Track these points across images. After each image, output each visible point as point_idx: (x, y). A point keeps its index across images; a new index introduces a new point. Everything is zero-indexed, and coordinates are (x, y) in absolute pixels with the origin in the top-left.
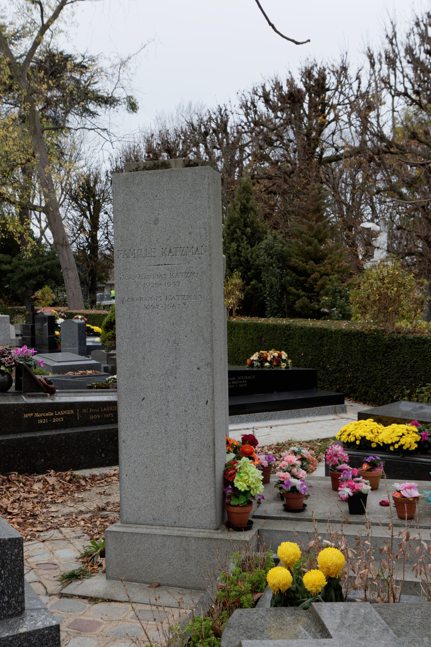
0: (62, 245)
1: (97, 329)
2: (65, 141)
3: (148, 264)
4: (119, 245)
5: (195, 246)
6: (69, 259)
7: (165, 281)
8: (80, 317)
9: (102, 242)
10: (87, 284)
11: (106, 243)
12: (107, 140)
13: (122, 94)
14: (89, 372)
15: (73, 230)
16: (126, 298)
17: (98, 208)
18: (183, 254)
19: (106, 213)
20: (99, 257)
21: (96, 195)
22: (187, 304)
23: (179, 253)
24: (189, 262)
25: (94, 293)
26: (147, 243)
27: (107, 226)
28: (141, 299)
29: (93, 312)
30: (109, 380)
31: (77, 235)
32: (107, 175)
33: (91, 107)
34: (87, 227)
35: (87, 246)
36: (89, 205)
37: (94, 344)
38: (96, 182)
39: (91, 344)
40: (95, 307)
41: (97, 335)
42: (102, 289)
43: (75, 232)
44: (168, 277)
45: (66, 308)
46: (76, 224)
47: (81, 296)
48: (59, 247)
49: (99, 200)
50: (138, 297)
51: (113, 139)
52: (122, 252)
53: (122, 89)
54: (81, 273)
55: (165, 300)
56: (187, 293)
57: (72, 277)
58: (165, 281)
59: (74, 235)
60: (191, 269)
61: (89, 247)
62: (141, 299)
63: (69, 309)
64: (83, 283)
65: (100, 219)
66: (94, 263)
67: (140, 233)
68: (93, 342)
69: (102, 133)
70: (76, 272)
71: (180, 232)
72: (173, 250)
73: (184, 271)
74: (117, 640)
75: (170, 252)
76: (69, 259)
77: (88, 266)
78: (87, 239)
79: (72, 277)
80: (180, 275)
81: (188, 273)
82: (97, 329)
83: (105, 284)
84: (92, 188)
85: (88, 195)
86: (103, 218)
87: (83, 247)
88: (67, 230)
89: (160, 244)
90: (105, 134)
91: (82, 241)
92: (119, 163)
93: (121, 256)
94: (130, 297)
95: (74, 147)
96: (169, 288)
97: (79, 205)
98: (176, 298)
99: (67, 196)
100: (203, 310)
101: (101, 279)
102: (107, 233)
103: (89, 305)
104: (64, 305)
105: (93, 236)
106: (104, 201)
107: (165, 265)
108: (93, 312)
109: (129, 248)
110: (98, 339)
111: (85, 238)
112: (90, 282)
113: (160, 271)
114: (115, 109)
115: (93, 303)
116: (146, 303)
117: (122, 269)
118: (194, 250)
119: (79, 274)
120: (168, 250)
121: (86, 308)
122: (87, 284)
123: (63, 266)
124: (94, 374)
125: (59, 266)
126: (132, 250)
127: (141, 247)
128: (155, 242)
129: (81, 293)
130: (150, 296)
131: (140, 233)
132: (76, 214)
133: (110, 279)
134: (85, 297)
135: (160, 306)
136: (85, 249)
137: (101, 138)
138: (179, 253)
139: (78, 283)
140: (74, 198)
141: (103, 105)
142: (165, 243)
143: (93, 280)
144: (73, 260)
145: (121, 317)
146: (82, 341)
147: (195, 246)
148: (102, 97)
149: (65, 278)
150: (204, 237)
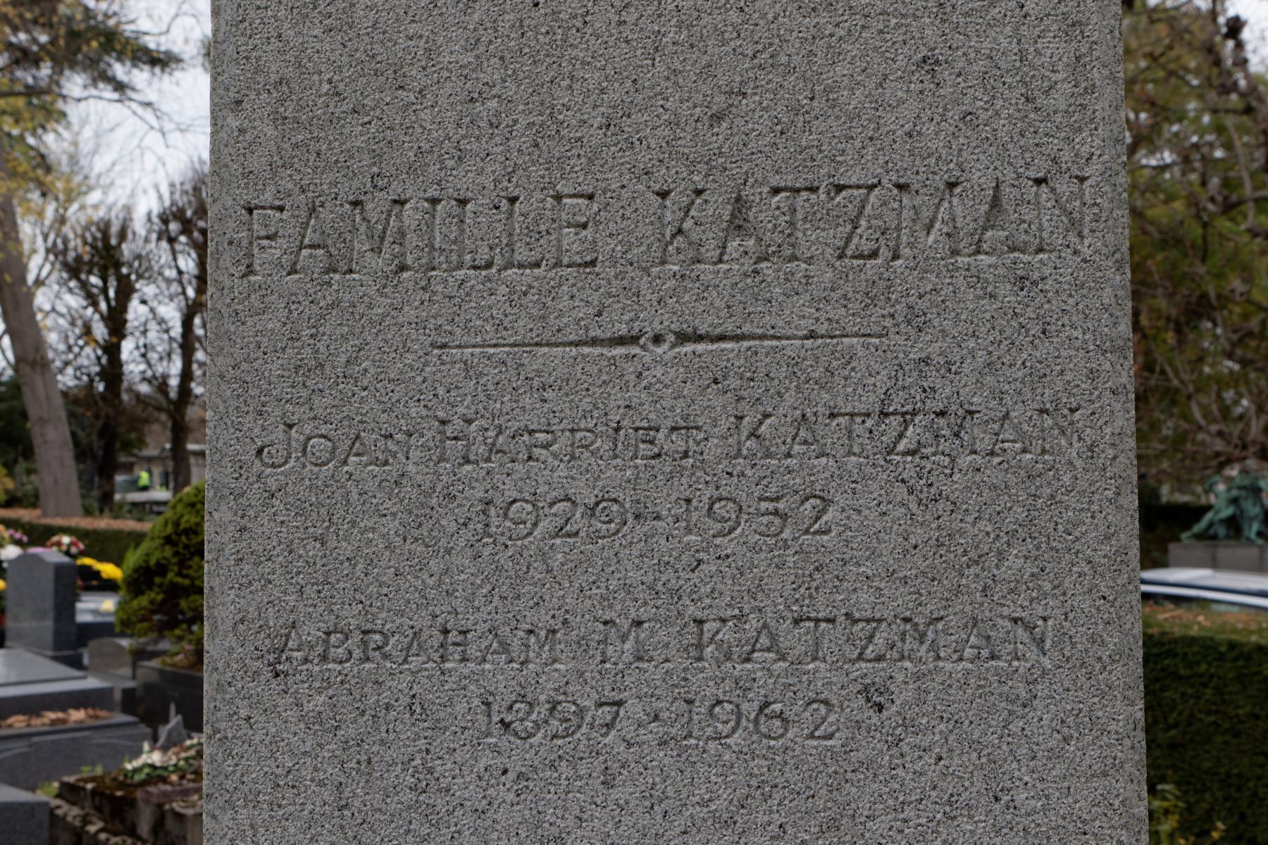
0: (33, 364)
1: (109, 570)
2: (53, 142)
3: (523, 327)
4: (257, 163)
5: (980, 177)
6: (48, 398)
7: (681, 488)
8: (66, 540)
9: (133, 365)
10: (94, 457)
11: (143, 367)
12: (152, 128)
13: (192, 29)
14: (77, 715)
15: (67, 337)
16: (311, 631)
17: (125, 291)
18: (861, 242)
19: (144, 302)
20: (125, 397)
21: (123, 264)
22: (905, 695)
23: (818, 240)
24: (917, 321)
25: (110, 478)
26: (521, 141)
27: (144, 332)
28: (451, 638)
29: (103, 523)
30: (136, 771)
31: (76, 349)
32: (149, 220)
33: (120, 70)
34: (100, 331)
35: (98, 374)
36: (105, 281)
37: (99, 619)
38: (122, 235)
39: (88, 618)
40: (111, 510)
41: (108, 586)
42: (129, 468)
43: (72, 341)
44: (713, 449)
45: (38, 512)
46: (73, 324)
47: (75, 486)
48: (26, 369)
49: (128, 276)
50: (422, 621)
51: (168, 126)
52: (287, 223)
53: (193, 21)
54: (81, 434)
55: (680, 662)
56: (899, 600)
57: (54, 441)
58: (681, 488)
59: (70, 348)
60: (934, 379)
61: (103, 374)
62: (451, 638)
63: (45, 515)
64: (82, 453)
65: (130, 316)
66: (111, 411)
67: (453, 53)
68: (96, 612)
69: (140, 110)
70: (65, 430)
71: (835, 57)
72: (767, 213)
73: (870, 402)
74: (148, 225)
75: (738, 225)
76: (48, 398)
77: (97, 417)
78: (99, 358)
79: (54, 441)
80: (832, 433)
81: (907, 418)
82: (109, 570)
83: (135, 456)
84: (114, 248)
85: (102, 262)
86: (136, 312)
87: (89, 375)
88: (52, 338)
89: (644, 158)
90: (148, 115)
91: (86, 362)
92: (177, 196)
93: (275, 251)
94: (351, 617)
95: (73, 159)
96: (727, 545)
97: (84, 285)
98: (795, 640)
99: (58, 266)
100: (1054, 755)
101: (127, 446)
102: (145, 346)
103: (96, 505)
104: (34, 506)
105: (112, 350)
106: (140, 277)
107: (683, 338)
108: (103, 523)
109: (348, 189)
110: (108, 604)
111: (93, 356)
112: (101, 453)
113: (637, 395)
114: (174, 79)
115: (106, 501)
116: (500, 678)
117: (275, 368)
118: (964, 210)
119: (73, 434)
120: (718, 206)
121: (88, 512)
122: (94, 457)
123: (33, 412)
124: (90, 723)
125: (24, 415)
126: (376, 206)
127: (463, 180)
128: (595, 136)
129: (74, 478)
130: (543, 619)
131: (453, 53)
132: (74, 301)
133: (147, 446)
134: (86, 484)
135: (634, 708)
136: (91, 381)
137: (138, 121)
138: (818, 240)
139: (69, 454)
140: (74, 269)
141: (147, 68)
142: (685, 144)
143: (109, 450)
144: (59, 401)
145: (253, 800)
146: (65, 608)
147: (980, 177)
148: (146, 51)
149: (37, 441)
150: (1059, 100)
